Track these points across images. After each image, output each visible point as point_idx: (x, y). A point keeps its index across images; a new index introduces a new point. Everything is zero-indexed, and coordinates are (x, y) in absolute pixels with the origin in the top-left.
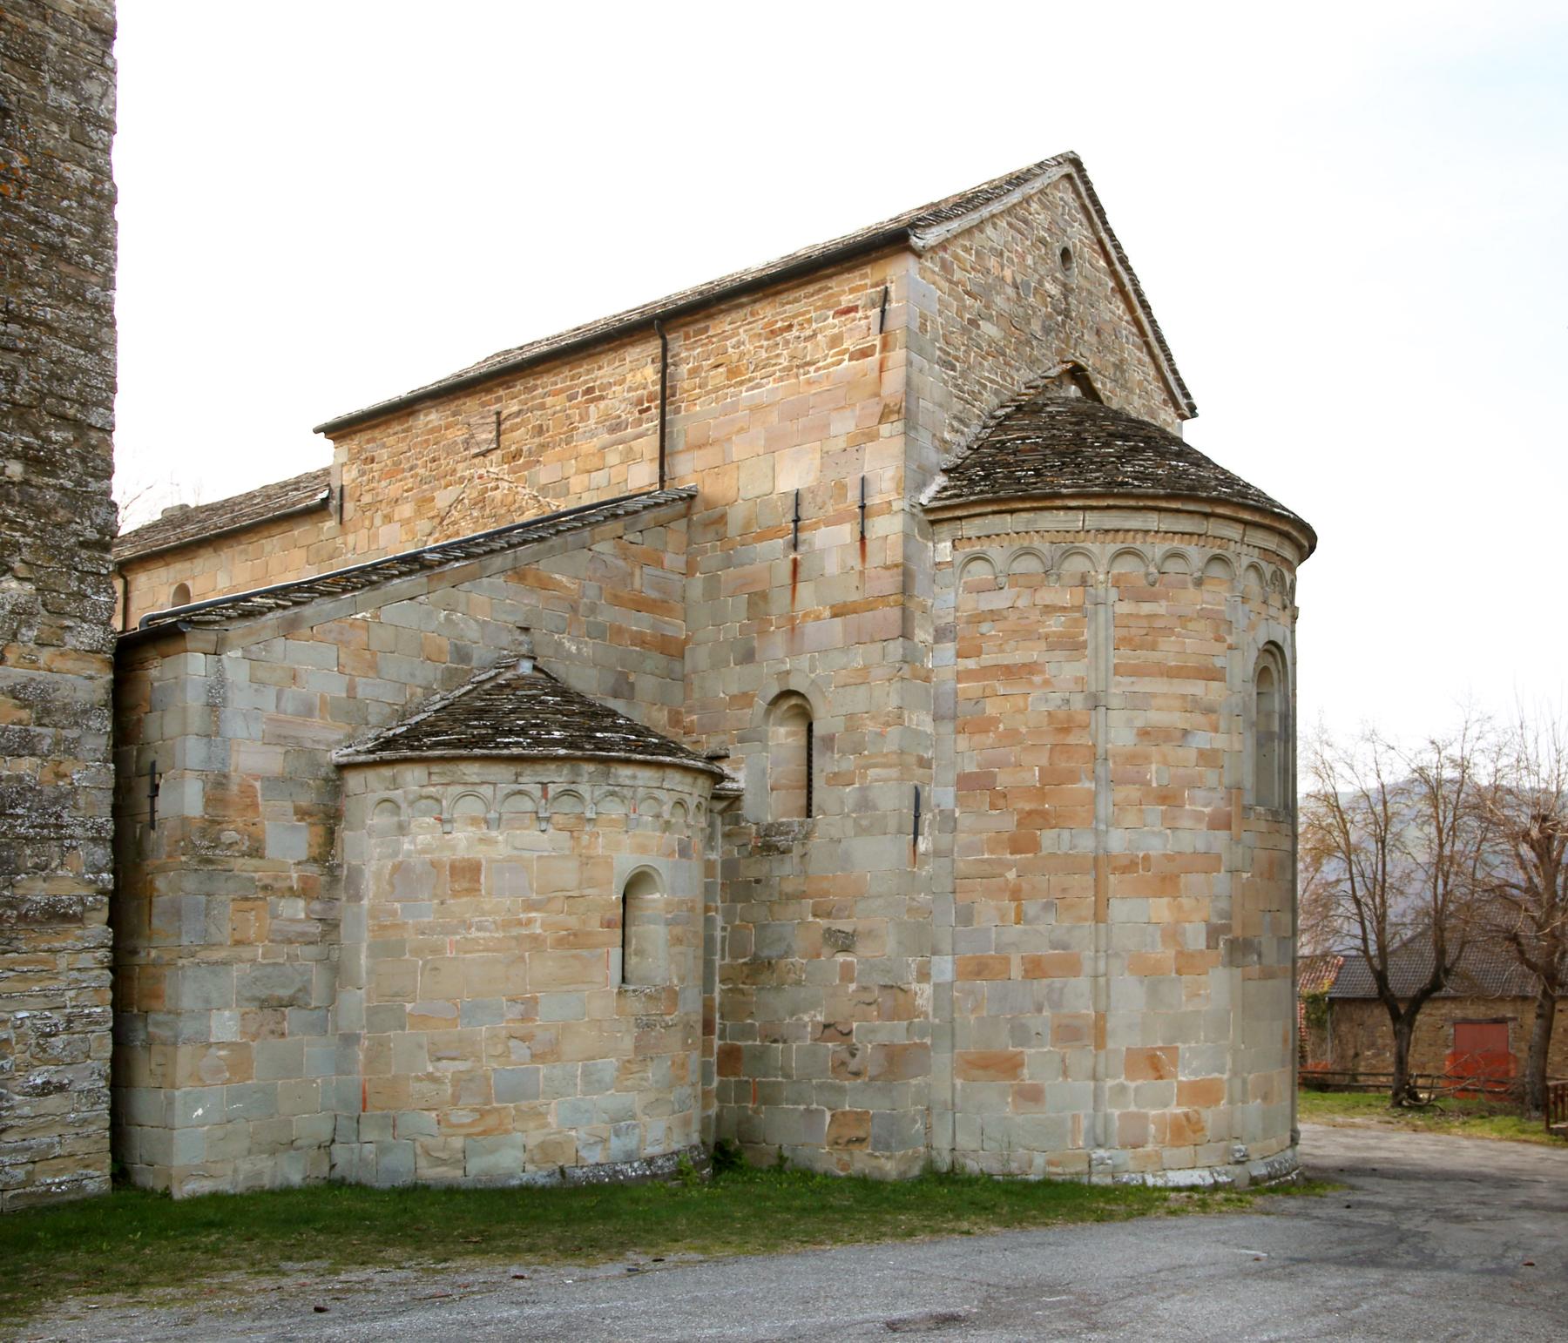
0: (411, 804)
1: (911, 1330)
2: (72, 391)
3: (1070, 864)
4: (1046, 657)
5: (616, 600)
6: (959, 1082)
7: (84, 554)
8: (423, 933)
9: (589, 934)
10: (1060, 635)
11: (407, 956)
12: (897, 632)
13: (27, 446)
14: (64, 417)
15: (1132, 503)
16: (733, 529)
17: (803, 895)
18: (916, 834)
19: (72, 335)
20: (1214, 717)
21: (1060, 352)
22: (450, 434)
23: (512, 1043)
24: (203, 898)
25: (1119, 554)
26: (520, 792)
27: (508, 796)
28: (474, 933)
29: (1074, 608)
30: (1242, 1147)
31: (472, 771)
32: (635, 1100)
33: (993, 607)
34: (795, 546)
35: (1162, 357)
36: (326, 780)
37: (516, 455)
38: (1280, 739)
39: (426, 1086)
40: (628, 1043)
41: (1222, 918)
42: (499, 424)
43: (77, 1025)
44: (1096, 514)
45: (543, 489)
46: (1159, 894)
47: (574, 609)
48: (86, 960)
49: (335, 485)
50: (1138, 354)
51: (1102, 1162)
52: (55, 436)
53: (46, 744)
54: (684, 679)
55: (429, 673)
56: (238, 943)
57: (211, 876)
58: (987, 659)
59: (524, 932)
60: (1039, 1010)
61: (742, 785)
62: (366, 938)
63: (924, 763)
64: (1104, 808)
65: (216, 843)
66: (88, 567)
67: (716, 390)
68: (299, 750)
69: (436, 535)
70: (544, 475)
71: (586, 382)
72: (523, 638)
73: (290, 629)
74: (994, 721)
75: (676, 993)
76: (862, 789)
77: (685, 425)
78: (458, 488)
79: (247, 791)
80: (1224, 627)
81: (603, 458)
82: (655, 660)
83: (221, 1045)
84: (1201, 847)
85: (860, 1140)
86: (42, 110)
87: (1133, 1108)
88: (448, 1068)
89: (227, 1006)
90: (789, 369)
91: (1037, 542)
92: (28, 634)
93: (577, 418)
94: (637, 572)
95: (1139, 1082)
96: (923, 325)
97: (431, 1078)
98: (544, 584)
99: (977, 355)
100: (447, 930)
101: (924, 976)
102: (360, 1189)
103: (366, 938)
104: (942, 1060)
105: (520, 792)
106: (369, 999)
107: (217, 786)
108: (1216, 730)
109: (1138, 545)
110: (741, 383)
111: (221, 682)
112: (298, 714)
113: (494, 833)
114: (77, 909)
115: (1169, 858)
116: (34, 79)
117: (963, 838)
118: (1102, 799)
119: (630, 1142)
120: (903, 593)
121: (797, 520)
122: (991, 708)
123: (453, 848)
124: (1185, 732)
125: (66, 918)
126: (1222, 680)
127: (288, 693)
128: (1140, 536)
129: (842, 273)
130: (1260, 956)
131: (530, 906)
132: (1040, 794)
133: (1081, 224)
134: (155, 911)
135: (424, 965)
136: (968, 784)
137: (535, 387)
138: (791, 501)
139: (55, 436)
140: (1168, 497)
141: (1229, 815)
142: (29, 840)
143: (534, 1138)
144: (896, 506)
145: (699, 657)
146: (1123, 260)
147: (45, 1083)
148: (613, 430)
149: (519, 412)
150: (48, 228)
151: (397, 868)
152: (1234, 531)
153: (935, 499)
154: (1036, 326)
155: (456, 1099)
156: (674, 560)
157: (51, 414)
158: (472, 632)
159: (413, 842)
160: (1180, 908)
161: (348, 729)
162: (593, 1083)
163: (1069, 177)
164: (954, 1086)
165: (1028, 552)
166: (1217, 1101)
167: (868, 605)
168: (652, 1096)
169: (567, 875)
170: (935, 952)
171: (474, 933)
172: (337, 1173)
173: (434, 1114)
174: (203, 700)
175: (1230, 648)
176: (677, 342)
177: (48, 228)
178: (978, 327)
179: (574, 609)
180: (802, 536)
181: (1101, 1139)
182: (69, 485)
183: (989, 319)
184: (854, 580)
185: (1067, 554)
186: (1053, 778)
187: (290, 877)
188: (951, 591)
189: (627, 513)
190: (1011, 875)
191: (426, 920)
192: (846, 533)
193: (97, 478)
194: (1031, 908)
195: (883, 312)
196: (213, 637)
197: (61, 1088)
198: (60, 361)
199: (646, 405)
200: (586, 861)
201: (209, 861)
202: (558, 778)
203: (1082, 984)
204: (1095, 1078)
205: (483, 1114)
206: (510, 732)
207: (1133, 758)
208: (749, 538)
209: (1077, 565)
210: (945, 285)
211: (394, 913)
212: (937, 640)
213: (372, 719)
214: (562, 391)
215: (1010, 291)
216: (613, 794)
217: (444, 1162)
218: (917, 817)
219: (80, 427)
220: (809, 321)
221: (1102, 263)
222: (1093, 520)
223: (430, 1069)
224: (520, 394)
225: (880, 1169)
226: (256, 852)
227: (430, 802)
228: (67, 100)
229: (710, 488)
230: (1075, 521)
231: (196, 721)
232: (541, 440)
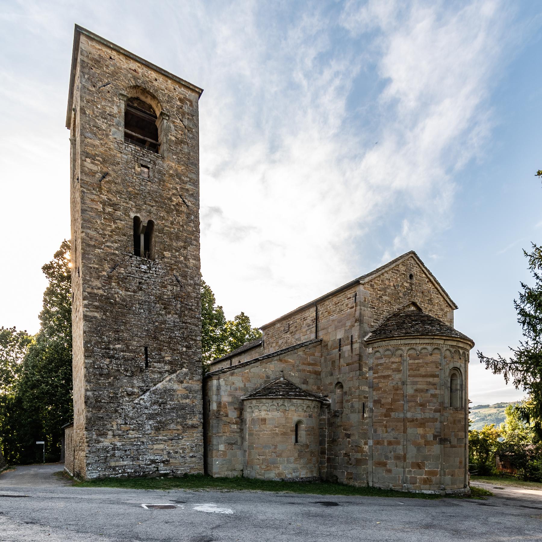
0: (254, 407)
3: (398, 420)
4: (393, 373)
5: (304, 364)
6: (374, 467)
7: (197, 363)
9: (287, 433)
10: (396, 368)
12: (358, 369)
13: (186, 345)
14: (192, 339)
15: (412, 337)
16: (329, 348)
17: (341, 426)
18: (363, 413)
19: (194, 324)
20: (435, 386)
21: (409, 299)
23: (273, 453)
25: (410, 349)
28: (265, 432)
29: (399, 362)
30: (443, 486)
31: (264, 401)
32: (299, 466)
33: (381, 362)
34: (340, 350)
35: (445, 295)
37: (292, 333)
38: (460, 390)
39: (257, 461)
40: (296, 455)
41: (437, 433)
43: (197, 446)
44: (404, 340)
45: (296, 339)
46: (420, 427)
48: (199, 435)
49: (263, 340)
50: (437, 296)
51: (405, 486)
52: (191, 342)
53: (191, 397)
54: (320, 379)
55: (261, 381)
56: (224, 432)
57: (218, 420)
58: (380, 374)
59: (274, 432)
60: (391, 452)
61: (331, 402)
63: (365, 397)
64: (406, 407)
65: (219, 414)
66: (197, 365)
67: (326, 317)
68: (234, 397)
72: (281, 373)
73: (232, 374)
74: (381, 388)
75: (308, 445)
76: (352, 403)
77: (320, 325)
78: (282, 340)
79: (225, 405)
80: (438, 365)
82: (313, 376)
83: (221, 451)
84: (431, 416)
85: (351, 478)
87: (413, 475)
88: (261, 457)
89: (222, 444)
90: (339, 312)
91: (390, 347)
92: (187, 378)
94: (309, 358)
95: (415, 470)
96: (365, 301)
97: (258, 459)
98: (286, 362)
99: (382, 304)
100: (261, 431)
101: (366, 444)
104: (370, 462)
107: (219, 404)
108: (436, 389)
109: (414, 347)
110: (330, 315)
111: (219, 385)
112: (234, 390)
114: (197, 426)
115: (423, 419)
116: (186, 279)
117: (374, 414)
118: (405, 406)
119: (297, 474)
120: (359, 360)
121: (340, 345)
122: (380, 385)
123: (261, 416)
124: (427, 390)
125: (195, 427)
126: (439, 377)
127: (232, 386)
128: (415, 345)
129: (348, 290)
130: (450, 442)
131: (276, 427)
132: (391, 404)
133: (416, 267)
136: (377, 402)
138: (338, 342)
139: (191, 342)
140: (420, 335)
141: (440, 409)
142: (188, 414)
143: (277, 472)
144: (358, 341)
145: (323, 375)
146: (430, 274)
148: (308, 327)
152: (442, 342)
153: (368, 339)
154: (401, 295)
155: (262, 463)
156: (317, 354)
158: (270, 373)
160: (426, 430)
161: (244, 393)
162: (289, 462)
163: (412, 257)
164: (373, 468)
165: (388, 350)
166: (436, 475)
167: (353, 363)
168: (302, 465)
169: (283, 421)
170: (369, 439)
171: (265, 432)
174: (216, 388)
175: (440, 369)
177: (189, 305)
178: (382, 298)
180: (341, 348)
181: (405, 482)
183: (386, 295)
184: (350, 358)
185: (397, 350)
186: (394, 401)
188: (372, 359)
189: (305, 346)
190: (385, 422)
192: (349, 347)
194: (389, 430)
195: (355, 298)
196: (217, 377)
197: (195, 457)
198: (192, 329)
200: (286, 418)
201: (218, 418)
202: (280, 402)
203: (401, 447)
204: (403, 468)
205: (267, 467)
206: (272, 393)
207: (413, 396)
208: (332, 349)
209: (400, 352)
210: (372, 290)
212: (369, 370)
213: (249, 391)
215: (393, 288)
216: (292, 405)
217: (261, 475)
218: (364, 409)
220: (342, 301)
221: (424, 275)
222: (403, 342)
225: (355, 484)
226: (227, 416)
228: (192, 282)
229: (325, 338)
230: (399, 342)
231: (215, 392)
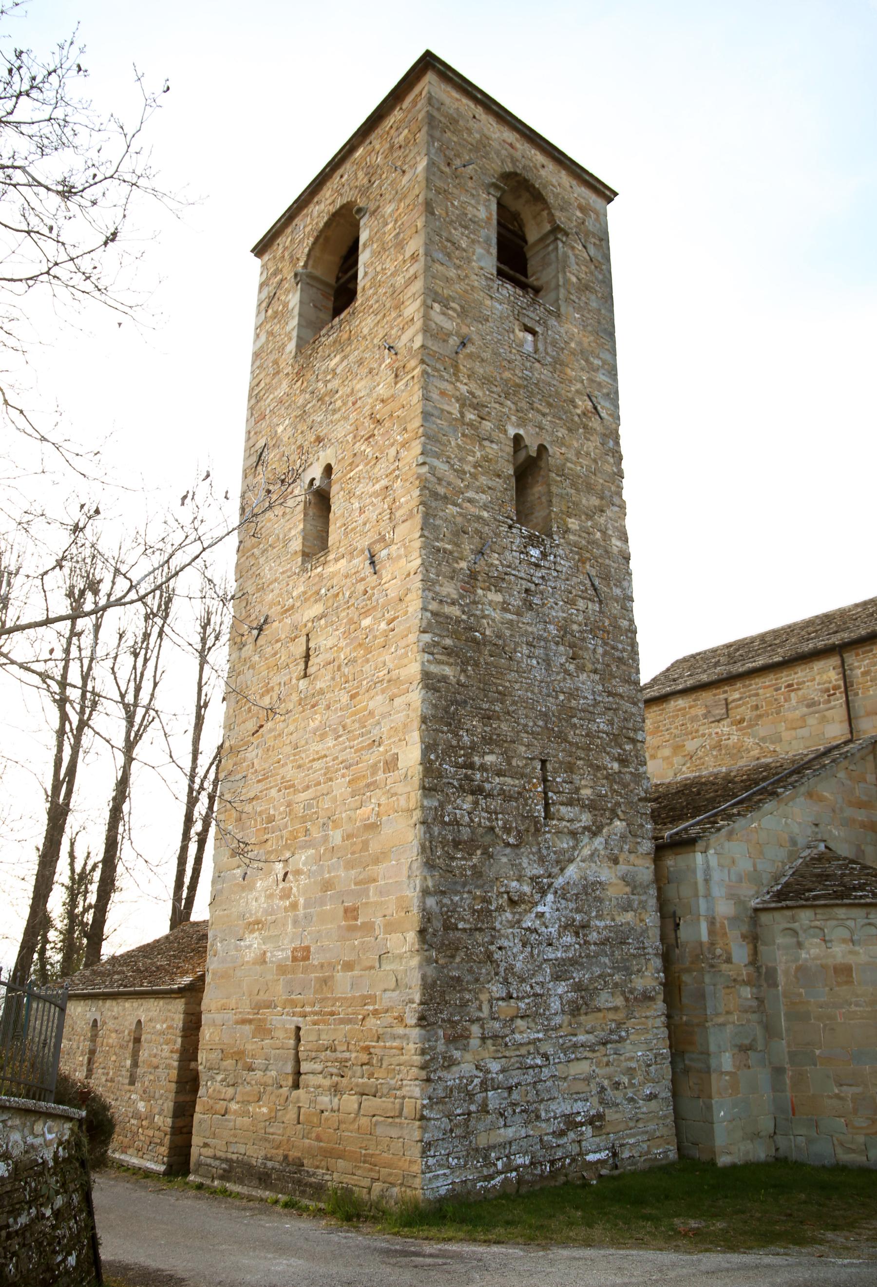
0: (805, 931)
1: (427, 1238)
2: (631, 725)
7: (641, 804)
8: (821, 1007)
11: (812, 1021)
13: (619, 754)
22: (693, 712)
24: (712, 987)
26: (870, 924)
27: (863, 926)
28: (853, 1008)
31: (841, 912)
36: (751, 917)
37: (742, 721)
42: (727, 704)
45: (763, 739)
47: (834, 811)
55: (783, 854)
62: (783, 1010)
69: (688, 765)
70: (762, 730)
71: (786, 681)
81: (805, 721)
83: (727, 1073)
86: (612, 598)
88: (849, 1091)
93: (782, 700)
97: (838, 1097)
98: (821, 799)
102: (798, 1165)
103: (783, 1010)
105: (870, 924)
106: (789, 1046)
113: (857, 948)
134: (683, 994)
135: (825, 1026)
137: (751, 685)
147: (651, 1093)
148: (808, 706)
149: (740, 699)
150: (618, 650)
151: (799, 969)
155: (855, 1111)
157: (626, 737)
158: (796, 829)
159: (808, 953)
171: (853, 1008)
172: (781, 1153)
173: (843, 1120)
176: (851, 658)
177: (618, 650)
179: (834, 811)
182: (633, 770)
187: (742, 974)
191: (822, 999)
193: (642, 766)
199: (832, 692)
211: (800, 995)
213: (765, 882)
214: (770, 686)
217: (853, 1151)
219: (634, 741)
223: (836, 1091)
224: (739, 688)
226: (729, 960)
227: (817, 930)
232: (758, 712)
